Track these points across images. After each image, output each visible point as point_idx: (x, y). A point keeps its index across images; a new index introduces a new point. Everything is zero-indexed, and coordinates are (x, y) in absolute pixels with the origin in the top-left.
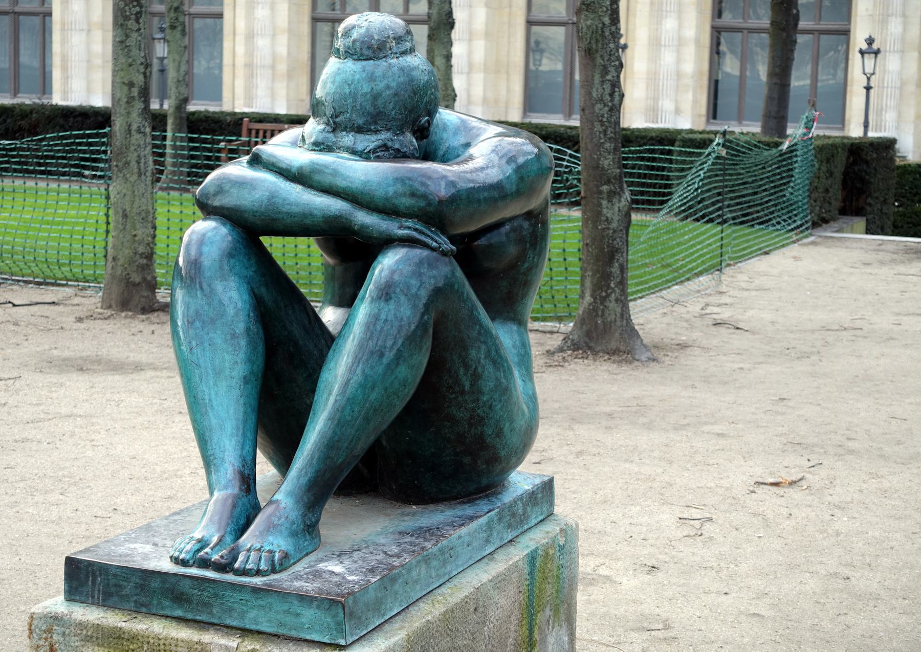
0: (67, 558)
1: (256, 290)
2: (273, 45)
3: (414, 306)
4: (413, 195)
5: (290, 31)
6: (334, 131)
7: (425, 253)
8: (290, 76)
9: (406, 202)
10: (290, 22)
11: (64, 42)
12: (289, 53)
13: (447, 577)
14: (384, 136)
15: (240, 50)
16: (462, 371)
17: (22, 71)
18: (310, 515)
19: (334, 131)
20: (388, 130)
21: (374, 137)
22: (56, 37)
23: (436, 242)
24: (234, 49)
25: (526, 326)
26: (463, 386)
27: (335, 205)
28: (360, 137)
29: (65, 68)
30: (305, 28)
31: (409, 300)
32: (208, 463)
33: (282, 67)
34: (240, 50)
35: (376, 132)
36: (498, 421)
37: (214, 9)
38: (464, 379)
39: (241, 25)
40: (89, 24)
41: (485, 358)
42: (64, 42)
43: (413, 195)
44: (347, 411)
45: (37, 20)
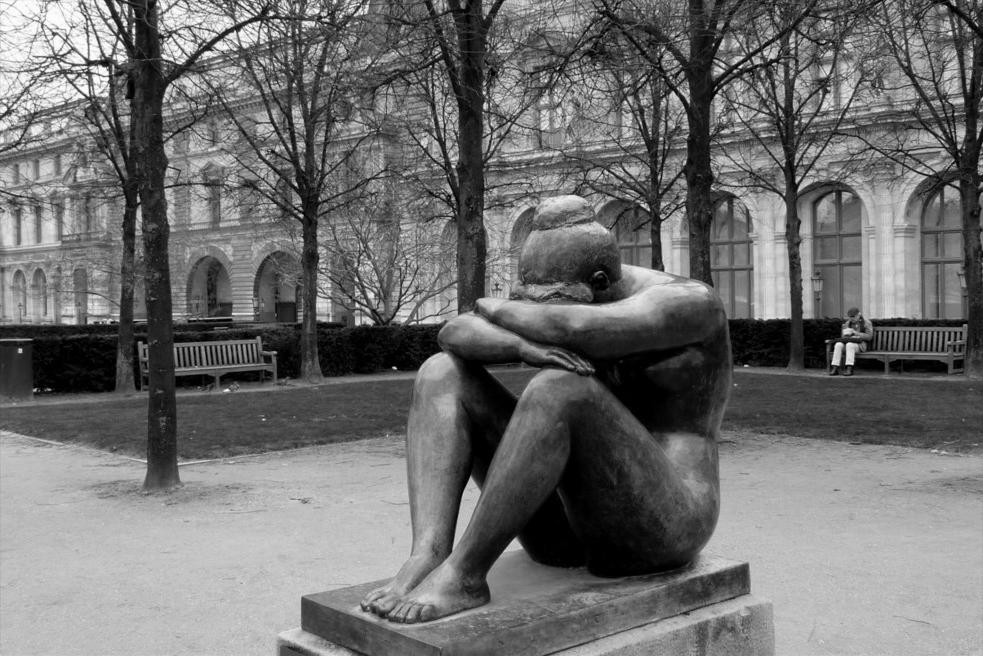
0: (771, 605)
1: (467, 405)
2: (894, 280)
3: (549, 414)
4: (556, 328)
5: (906, 271)
6: (524, 284)
7: (561, 373)
8: (907, 299)
9: (550, 333)
10: (906, 265)
11: (760, 286)
12: (906, 285)
13: (591, 638)
14: (559, 286)
15: (873, 284)
16: (608, 470)
17: (737, 305)
18: (469, 579)
19: (524, 284)
20: (562, 281)
21: (549, 287)
22: (756, 281)
23: (573, 364)
24: (869, 284)
25: (717, 439)
26: (611, 482)
27: (510, 338)
28: (539, 287)
29: (761, 301)
30: (917, 269)
31: (544, 409)
32: (416, 534)
33: (901, 294)
34: (873, 284)
35: (552, 283)
36: (652, 512)
37: (856, 260)
38: (611, 476)
39: (873, 268)
40: (776, 273)
41: (630, 459)
42: (760, 286)
43: (556, 328)
44: (494, 498)
45: (745, 273)
